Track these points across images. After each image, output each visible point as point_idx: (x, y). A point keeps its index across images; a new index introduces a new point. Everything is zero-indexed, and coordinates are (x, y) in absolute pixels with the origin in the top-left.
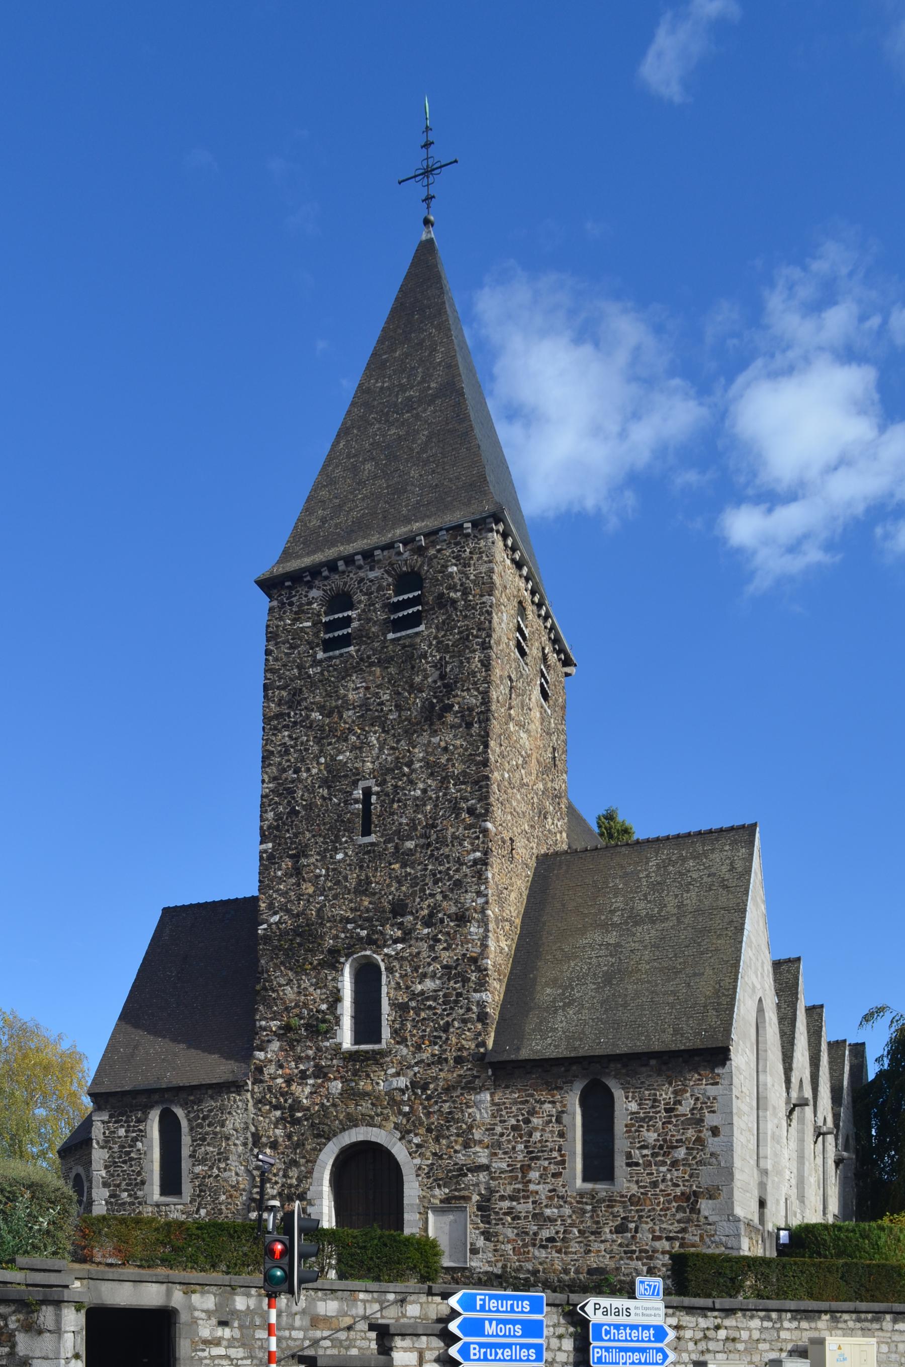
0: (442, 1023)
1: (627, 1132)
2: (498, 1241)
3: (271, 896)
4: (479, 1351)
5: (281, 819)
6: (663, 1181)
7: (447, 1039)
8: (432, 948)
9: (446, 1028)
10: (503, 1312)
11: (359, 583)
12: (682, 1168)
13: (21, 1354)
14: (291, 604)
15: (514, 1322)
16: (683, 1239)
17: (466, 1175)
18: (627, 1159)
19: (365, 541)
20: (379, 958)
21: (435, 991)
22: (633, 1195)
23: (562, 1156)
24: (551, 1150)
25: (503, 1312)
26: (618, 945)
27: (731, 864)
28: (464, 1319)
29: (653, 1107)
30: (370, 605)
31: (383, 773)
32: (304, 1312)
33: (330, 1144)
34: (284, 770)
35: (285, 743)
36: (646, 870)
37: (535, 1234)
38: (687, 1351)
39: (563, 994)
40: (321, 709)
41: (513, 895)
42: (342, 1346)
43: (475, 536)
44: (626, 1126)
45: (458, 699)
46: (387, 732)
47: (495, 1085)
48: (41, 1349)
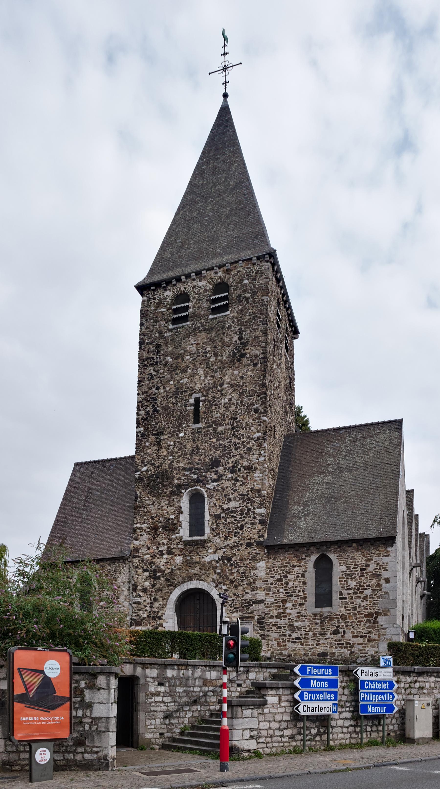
0: (239, 525)
1: (340, 581)
2: (269, 640)
3: (143, 456)
4: (308, 696)
5: (149, 414)
6: (359, 607)
7: (242, 533)
8: (234, 485)
9: (242, 528)
10: (320, 675)
11: (193, 288)
12: (369, 600)
13: (87, 701)
14: (154, 299)
15: (324, 680)
16: (369, 637)
17: (252, 605)
18: (340, 595)
19: (197, 266)
20: (203, 490)
21: (236, 508)
22: (343, 614)
23: (304, 594)
24: (299, 592)
25: (320, 675)
26: (332, 483)
27: (390, 440)
28: (302, 679)
29: (354, 568)
30: (199, 300)
31: (205, 391)
32: (200, 678)
33: (176, 590)
34: (151, 388)
35: (151, 374)
36: (345, 443)
37: (290, 636)
38: (401, 694)
39: (304, 509)
40: (171, 354)
41: (275, 456)
42: (218, 695)
43: (258, 265)
44: (340, 578)
45: (248, 351)
46: (209, 368)
47: (268, 557)
48: (99, 699)
